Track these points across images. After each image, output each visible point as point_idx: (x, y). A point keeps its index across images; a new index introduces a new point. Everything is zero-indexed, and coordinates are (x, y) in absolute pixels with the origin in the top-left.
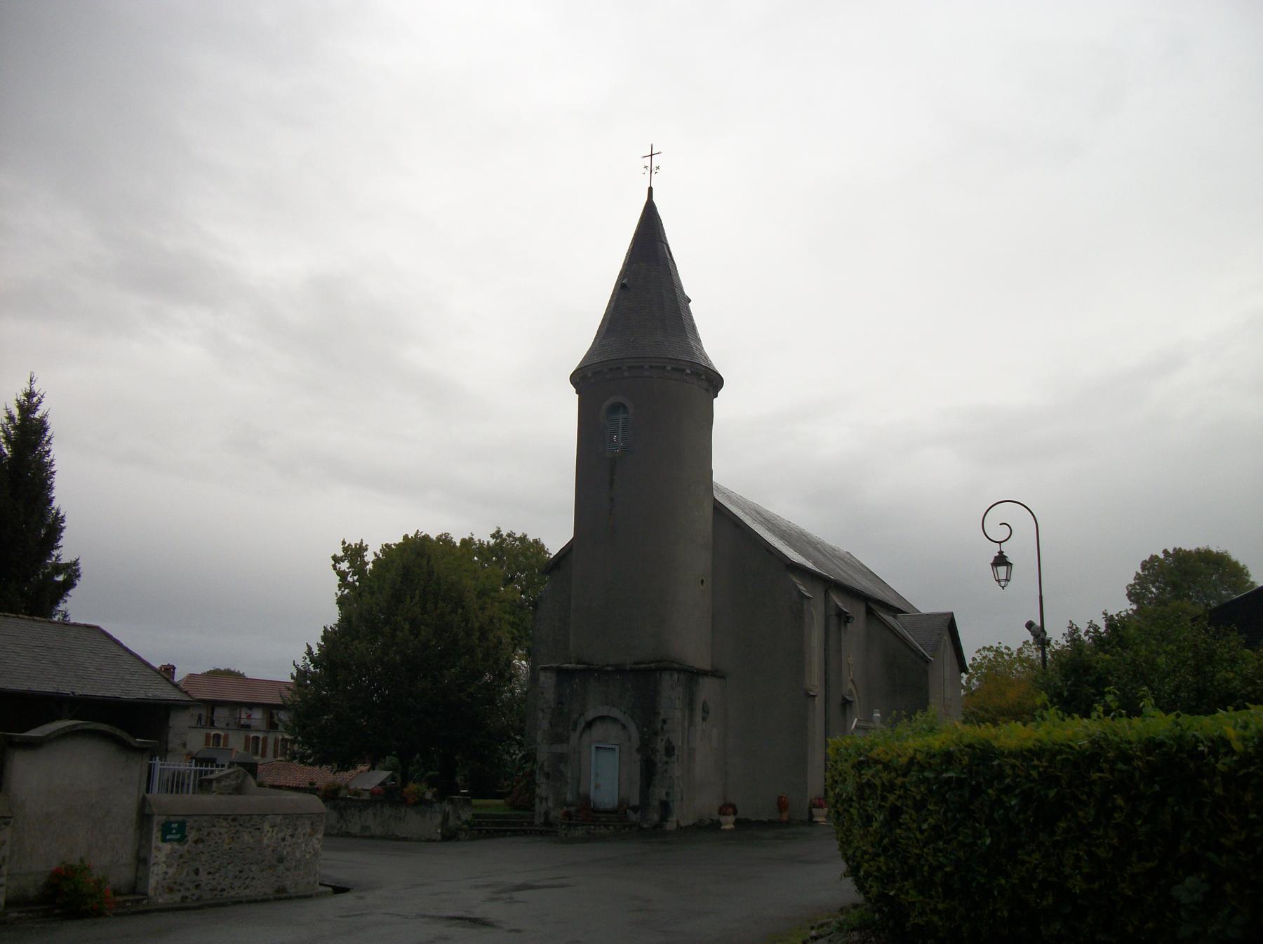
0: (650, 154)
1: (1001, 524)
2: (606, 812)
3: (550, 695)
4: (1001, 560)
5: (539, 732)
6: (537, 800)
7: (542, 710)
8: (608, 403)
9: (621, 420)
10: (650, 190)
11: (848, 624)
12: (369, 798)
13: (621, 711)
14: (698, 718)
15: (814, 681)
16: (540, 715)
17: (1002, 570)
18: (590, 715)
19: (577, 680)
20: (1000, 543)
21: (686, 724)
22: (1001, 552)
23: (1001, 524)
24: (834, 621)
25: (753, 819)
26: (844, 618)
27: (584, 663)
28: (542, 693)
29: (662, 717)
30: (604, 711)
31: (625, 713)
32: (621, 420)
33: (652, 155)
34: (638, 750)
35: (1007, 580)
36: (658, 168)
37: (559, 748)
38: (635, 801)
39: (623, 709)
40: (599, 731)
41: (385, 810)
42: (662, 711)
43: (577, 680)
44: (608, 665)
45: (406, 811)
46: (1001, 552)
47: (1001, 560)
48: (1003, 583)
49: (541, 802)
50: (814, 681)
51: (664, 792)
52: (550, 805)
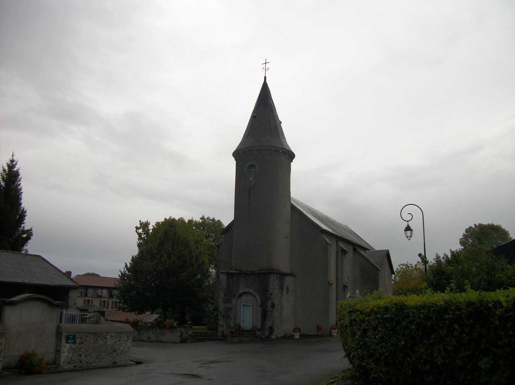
0: (265, 63)
1: (408, 214)
2: (247, 331)
3: (224, 284)
4: (408, 229)
5: (220, 299)
6: (219, 326)
7: (221, 290)
8: (248, 164)
9: (253, 171)
10: (265, 77)
11: (346, 254)
12: (150, 326)
13: (253, 290)
14: (285, 293)
15: (332, 278)
16: (220, 291)
17: (409, 232)
18: (241, 292)
19: (235, 278)
20: (408, 221)
21: (280, 295)
22: (408, 225)
23: (408, 214)
24: (340, 253)
25: (307, 334)
26: (344, 252)
27: (238, 271)
28: (221, 283)
29: (270, 292)
30: (246, 290)
31: (255, 291)
32: (253, 171)
33: (266, 63)
34: (260, 306)
35: (411, 237)
36: (268, 68)
37: (228, 305)
38: (259, 327)
39: (254, 289)
40: (244, 298)
41: (157, 330)
42: (270, 290)
43: (235, 278)
44: (248, 271)
45: (165, 331)
46: (408, 225)
47: (408, 229)
48: (409, 238)
49: (221, 327)
50: (332, 278)
51: (271, 323)
52: (224, 328)
